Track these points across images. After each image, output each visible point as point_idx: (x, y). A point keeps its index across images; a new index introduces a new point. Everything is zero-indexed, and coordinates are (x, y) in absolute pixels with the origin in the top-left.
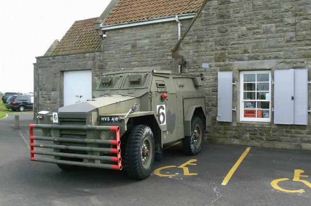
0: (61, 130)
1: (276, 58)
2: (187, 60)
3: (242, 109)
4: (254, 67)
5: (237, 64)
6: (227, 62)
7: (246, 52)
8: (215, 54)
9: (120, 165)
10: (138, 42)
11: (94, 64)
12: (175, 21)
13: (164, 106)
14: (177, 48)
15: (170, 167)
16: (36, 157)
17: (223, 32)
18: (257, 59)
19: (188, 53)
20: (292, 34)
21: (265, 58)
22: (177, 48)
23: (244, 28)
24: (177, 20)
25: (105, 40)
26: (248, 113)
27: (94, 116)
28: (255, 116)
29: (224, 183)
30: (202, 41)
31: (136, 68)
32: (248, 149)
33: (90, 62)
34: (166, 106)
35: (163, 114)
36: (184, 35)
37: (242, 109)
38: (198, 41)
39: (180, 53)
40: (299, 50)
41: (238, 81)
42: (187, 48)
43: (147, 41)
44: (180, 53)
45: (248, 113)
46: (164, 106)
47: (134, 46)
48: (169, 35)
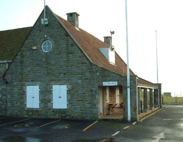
2: (8, 81)
6: (23, 82)
7: (30, 78)
8: (19, 79)
14: (4, 75)
15: (90, 126)
18: (34, 81)
19: (9, 78)
20: (46, 72)
22: (4, 75)
25: (35, 52)
29: (84, 130)
30: (14, 73)
31: (99, 66)
32: (136, 122)
36: (8, 68)
38: (12, 73)
39: (6, 78)
40: (48, 78)
44: (6, 78)
48: (3, 69)
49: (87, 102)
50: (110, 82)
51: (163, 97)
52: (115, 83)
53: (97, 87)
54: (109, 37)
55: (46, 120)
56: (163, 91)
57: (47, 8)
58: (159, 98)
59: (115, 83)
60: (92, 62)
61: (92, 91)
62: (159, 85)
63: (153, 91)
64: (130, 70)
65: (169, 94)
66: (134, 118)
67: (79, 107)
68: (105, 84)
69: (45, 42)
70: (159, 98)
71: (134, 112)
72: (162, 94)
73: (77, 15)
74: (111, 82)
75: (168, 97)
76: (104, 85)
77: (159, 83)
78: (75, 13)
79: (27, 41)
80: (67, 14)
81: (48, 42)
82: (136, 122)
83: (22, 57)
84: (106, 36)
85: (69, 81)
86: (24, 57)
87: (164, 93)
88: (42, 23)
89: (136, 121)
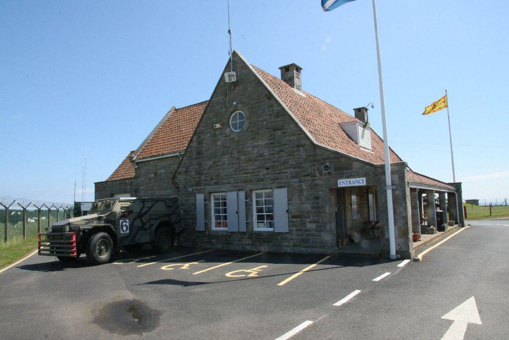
0: (53, 236)
1: (229, 183)
3: (213, 221)
4: (216, 190)
5: (208, 188)
6: (202, 187)
7: (212, 179)
9: (75, 254)
10: (159, 171)
11: (132, 188)
12: (177, 156)
13: (128, 221)
14: (174, 178)
16: (42, 252)
17: (200, 165)
21: (223, 184)
22: (174, 178)
23: (211, 162)
24: (179, 155)
26: (218, 224)
27: (67, 228)
28: (221, 226)
33: (129, 187)
34: (129, 220)
35: (126, 226)
37: (213, 221)
39: (177, 181)
41: (210, 200)
42: (180, 177)
43: (163, 171)
45: (218, 224)
46: (128, 221)
47: (156, 174)
49: (308, 220)
50: (352, 180)
51: (465, 207)
52: (361, 182)
53: (328, 190)
54: (362, 108)
55: (163, 271)
56: (466, 196)
57: (234, 54)
58: (458, 208)
59: (361, 182)
60: (316, 142)
61: (317, 198)
62: (458, 186)
63: (446, 195)
64: (389, 147)
65: (475, 202)
66: (404, 252)
67: (294, 229)
68: (343, 183)
69: (233, 115)
70: (458, 208)
71: (402, 240)
72: (464, 201)
73: (298, 69)
74: (354, 180)
75: (474, 206)
76: (339, 186)
77: (456, 182)
78: (293, 65)
79: (207, 115)
80: (280, 68)
81: (239, 113)
82: (406, 261)
83: (199, 144)
84: (358, 107)
85: (277, 181)
86: (203, 143)
87: (468, 201)
88: (227, 80)
89: (408, 257)
